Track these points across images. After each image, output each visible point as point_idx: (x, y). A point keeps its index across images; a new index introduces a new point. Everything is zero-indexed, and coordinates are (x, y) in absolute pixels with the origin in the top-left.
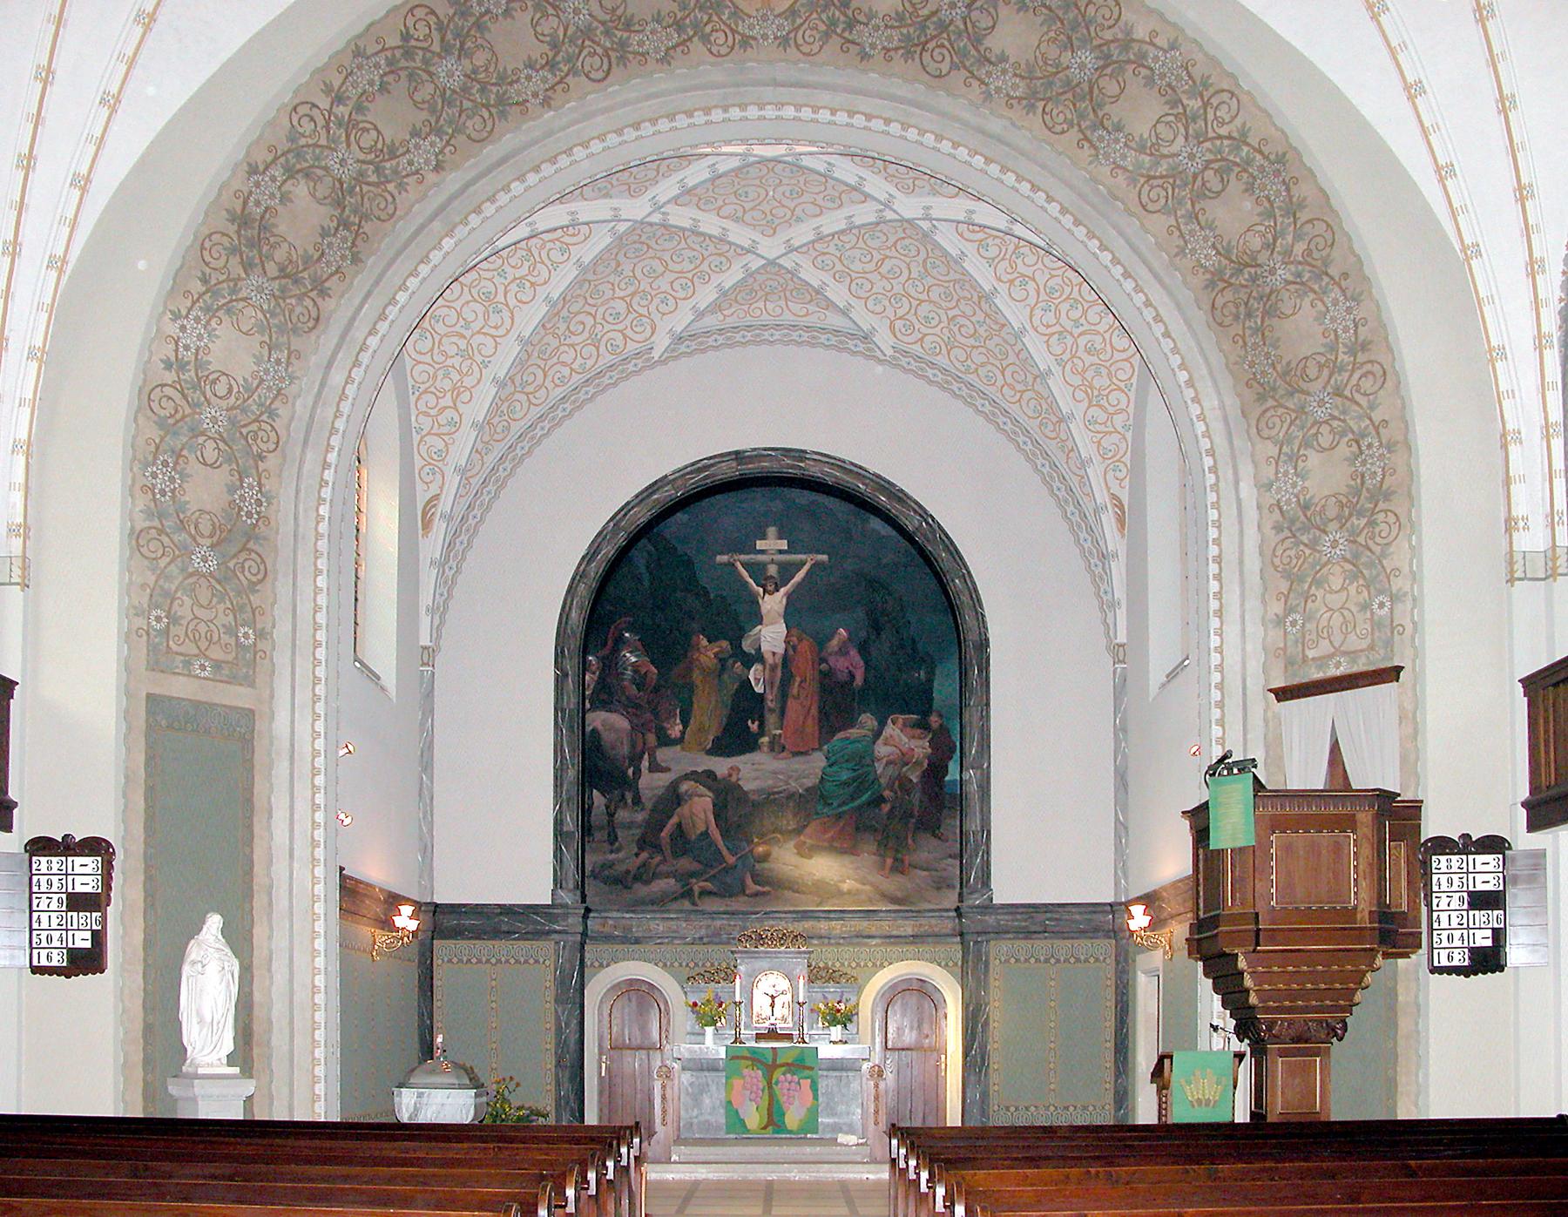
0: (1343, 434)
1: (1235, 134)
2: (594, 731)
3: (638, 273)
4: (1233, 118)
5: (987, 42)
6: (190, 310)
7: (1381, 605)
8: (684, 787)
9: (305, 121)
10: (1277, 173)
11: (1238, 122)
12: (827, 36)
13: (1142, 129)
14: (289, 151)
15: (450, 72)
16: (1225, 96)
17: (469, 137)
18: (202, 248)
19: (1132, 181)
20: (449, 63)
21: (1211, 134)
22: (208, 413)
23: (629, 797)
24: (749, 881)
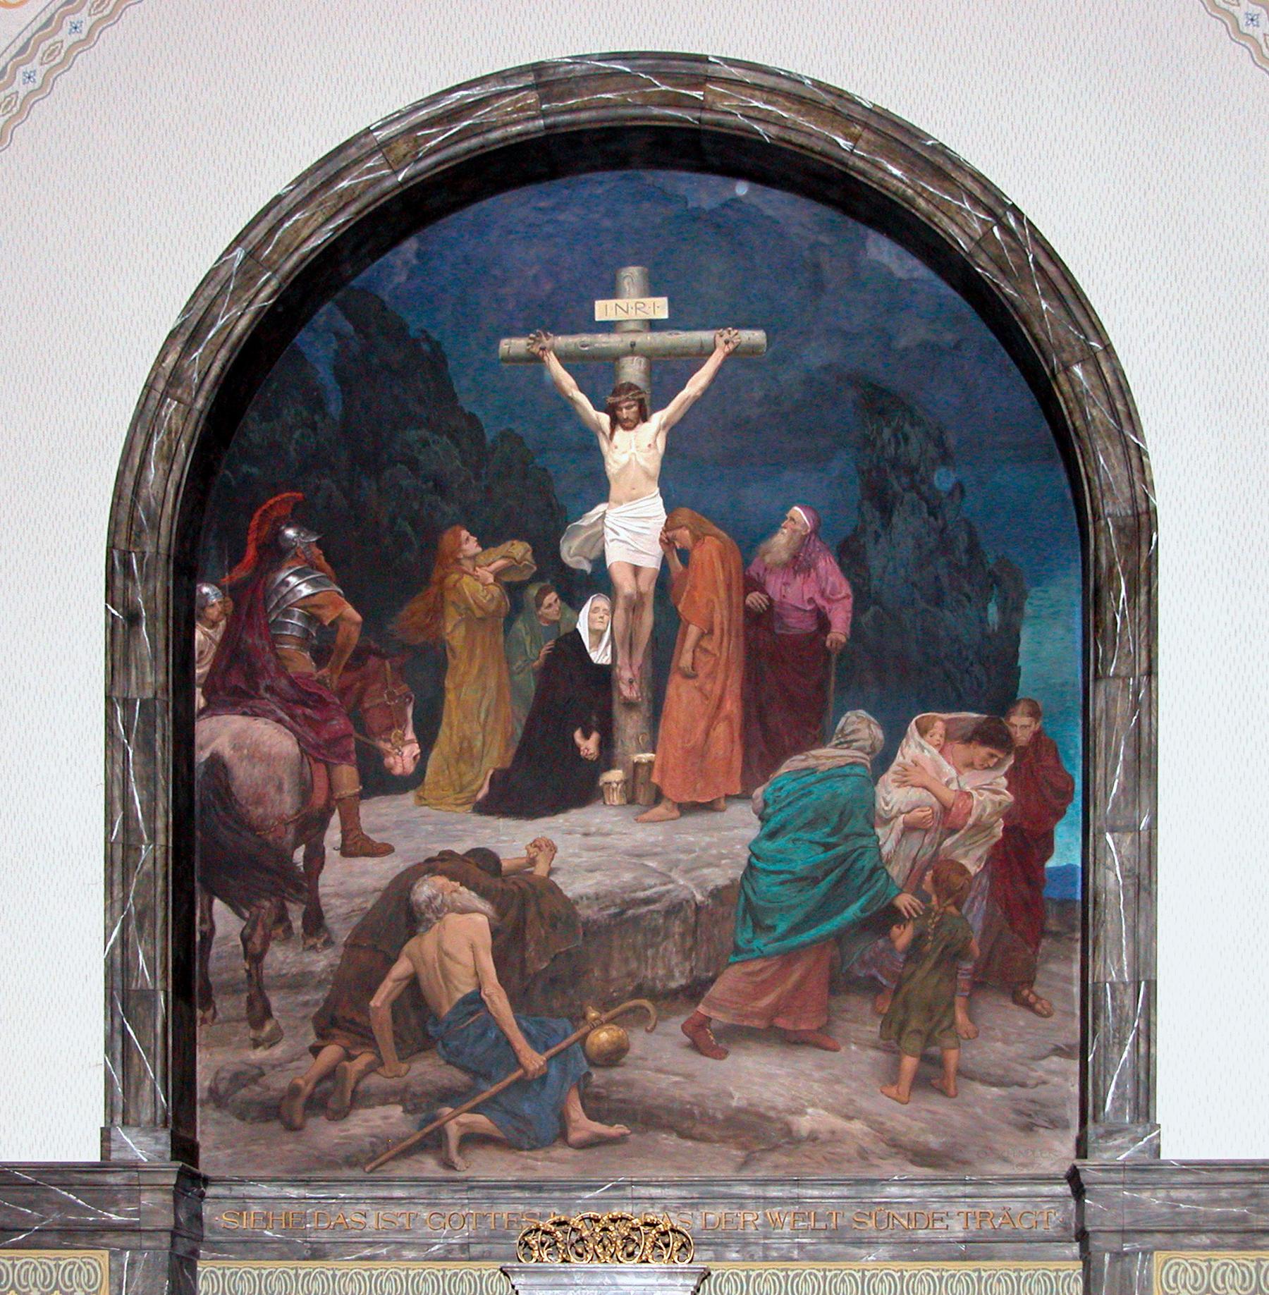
23: (296, 914)
24: (576, 1112)
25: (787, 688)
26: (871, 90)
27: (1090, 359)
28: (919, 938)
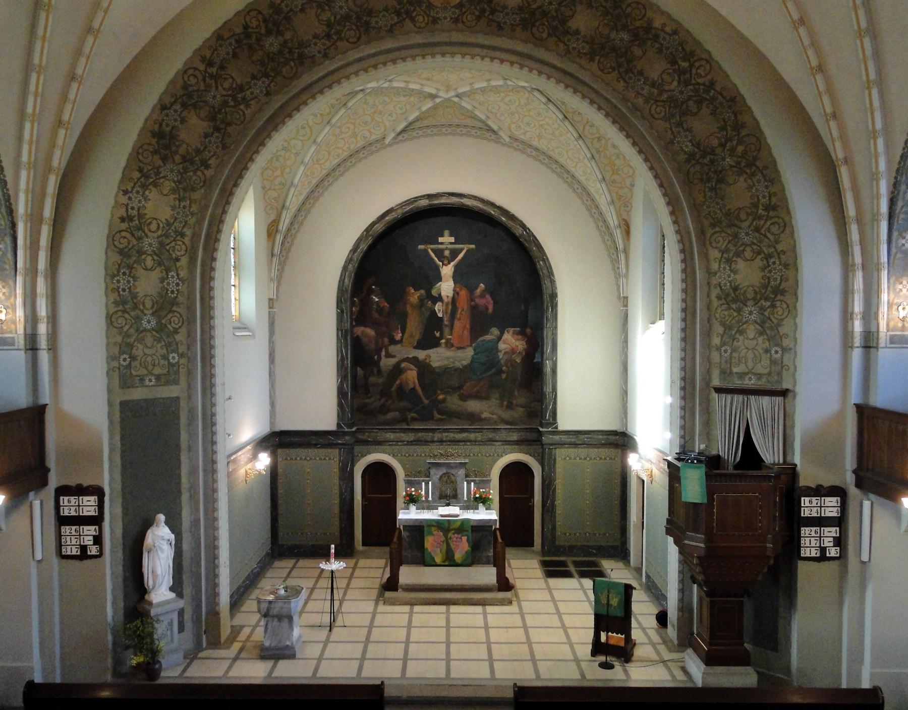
0: (759, 253)
1: (707, 83)
2: (358, 336)
3: (377, 103)
4: (706, 75)
5: (569, 24)
6: (133, 188)
7: (776, 352)
8: (403, 365)
9: (191, 78)
10: (730, 107)
11: (709, 77)
12: (479, 18)
13: (654, 75)
14: (184, 95)
15: (272, 44)
16: (703, 63)
17: (284, 77)
18: (138, 153)
19: (647, 101)
20: (271, 40)
21: (693, 82)
22: (147, 241)
23: (375, 370)
24: (435, 413)
25: (480, 323)
26: (499, 202)
27: (543, 260)
28: (507, 377)
